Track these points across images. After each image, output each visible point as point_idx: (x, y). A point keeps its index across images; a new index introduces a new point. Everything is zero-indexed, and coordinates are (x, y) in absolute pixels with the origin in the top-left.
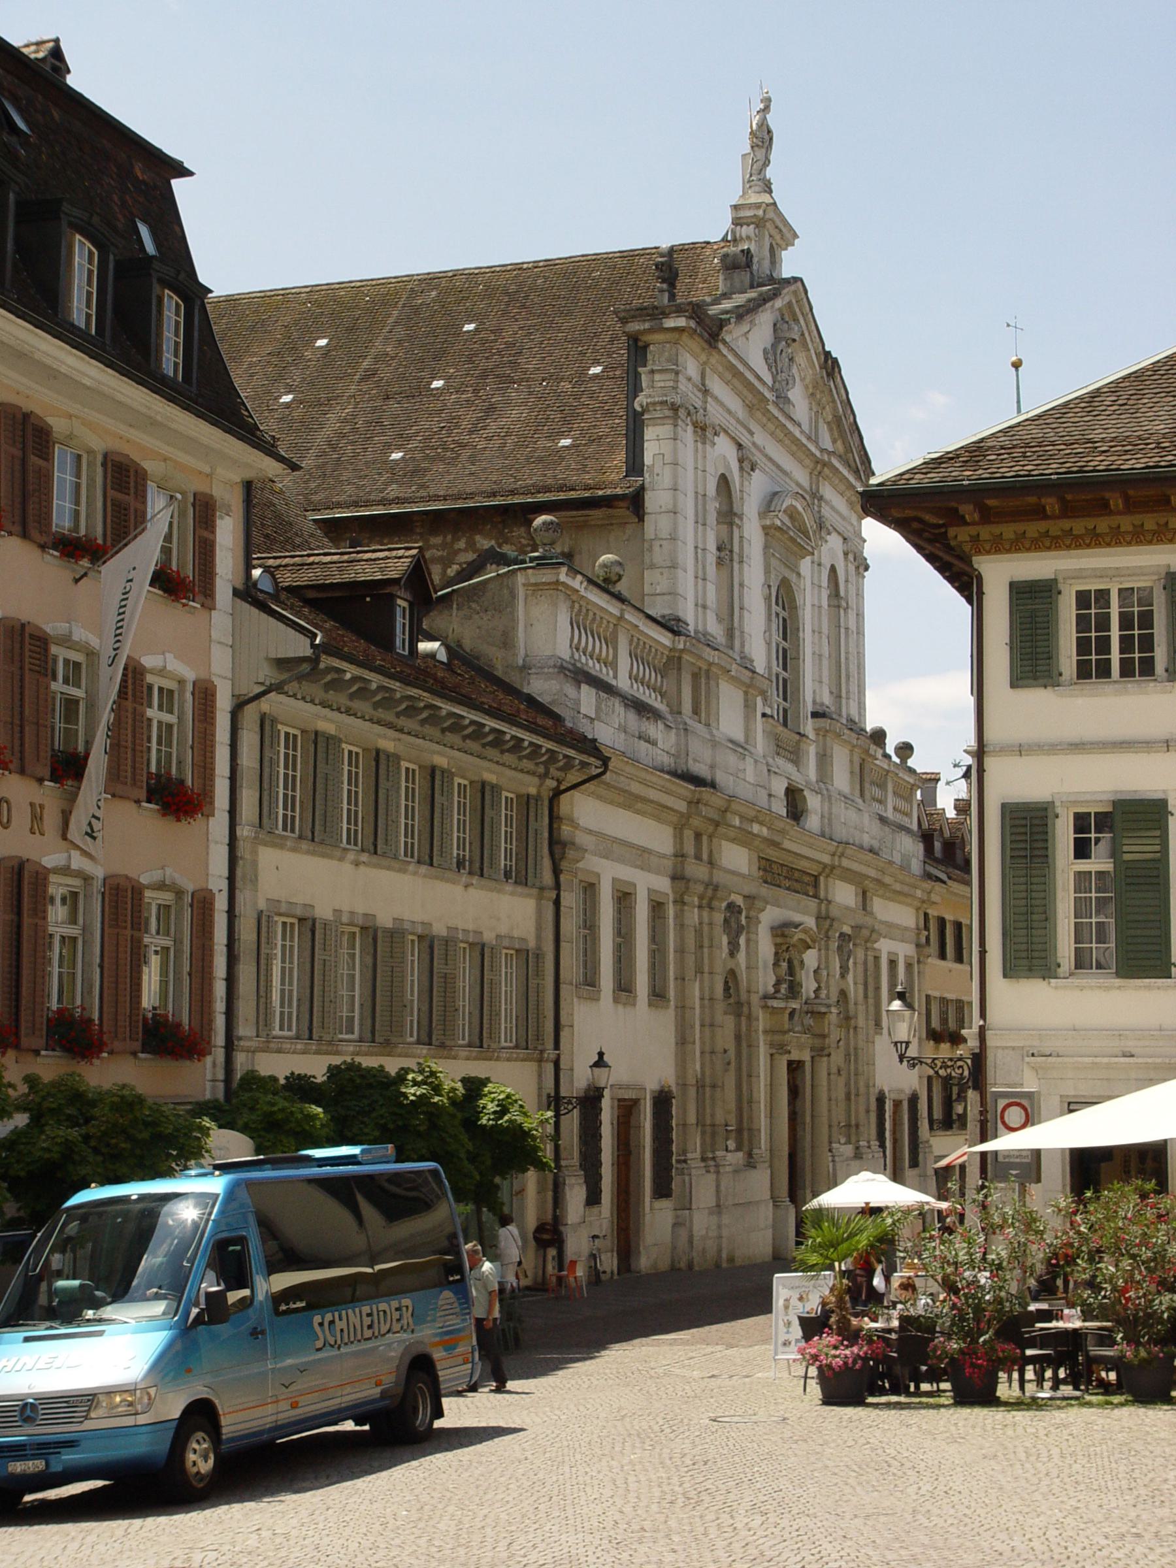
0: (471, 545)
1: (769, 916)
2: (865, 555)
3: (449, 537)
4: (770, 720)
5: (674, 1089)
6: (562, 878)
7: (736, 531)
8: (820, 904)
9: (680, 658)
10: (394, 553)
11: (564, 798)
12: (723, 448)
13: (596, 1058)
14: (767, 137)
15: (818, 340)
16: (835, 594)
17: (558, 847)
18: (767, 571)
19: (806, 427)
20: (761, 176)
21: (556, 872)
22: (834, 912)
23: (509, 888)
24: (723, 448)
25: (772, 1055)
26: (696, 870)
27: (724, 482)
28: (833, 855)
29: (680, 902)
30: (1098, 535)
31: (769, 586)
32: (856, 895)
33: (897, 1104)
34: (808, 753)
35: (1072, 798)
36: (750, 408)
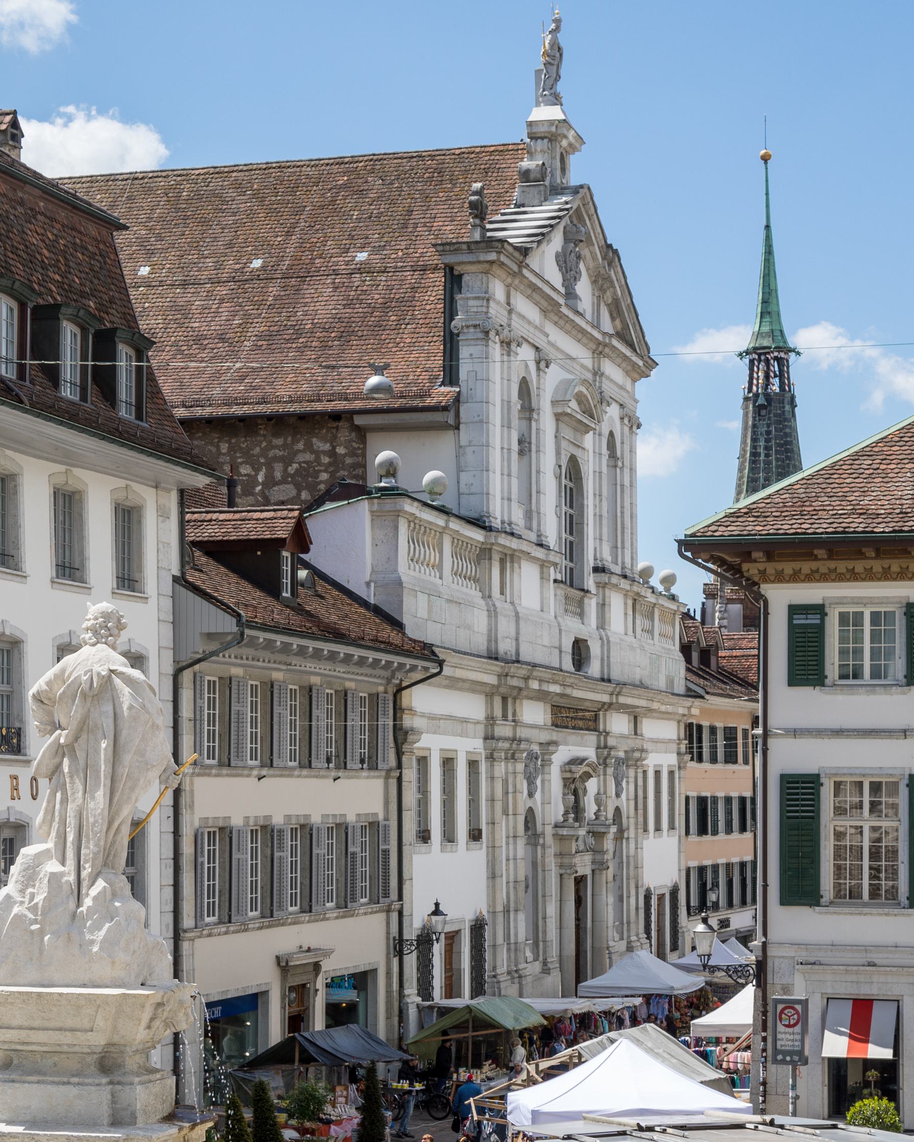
0: (309, 447)
1: (561, 755)
2: (637, 415)
3: (290, 439)
4: (561, 585)
5: (486, 917)
6: (404, 759)
7: (534, 424)
8: (599, 736)
9: (490, 550)
10: (279, 514)
11: (404, 693)
12: (525, 353)
13: (433, 908)
14: (558, 55)
15: (601, 236)
16: (613, 455)
17: (401, 735)
18: (558, 453)
19: (589, 316)
20: (552, 91)
21: (399, 754)
22: (611, 742)
23: (364, 774)
24: (525, 353)
25: (561, 875)
26: (503, 730)
27: (524, 385)
28: (612, 694)
29: (491, 758)
30: (856, 574)
31: (560, 466)
32: (629, 722)
33: (661, 898)
34: (590, 605)
35: (833, 771)
36: (544, 312)
